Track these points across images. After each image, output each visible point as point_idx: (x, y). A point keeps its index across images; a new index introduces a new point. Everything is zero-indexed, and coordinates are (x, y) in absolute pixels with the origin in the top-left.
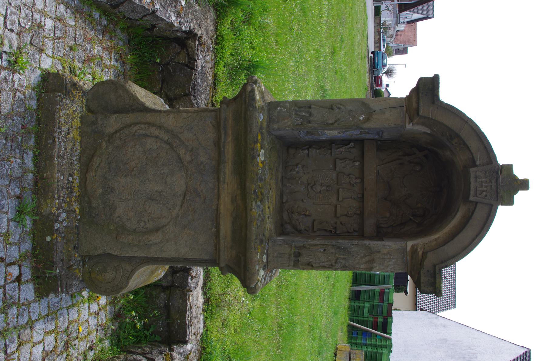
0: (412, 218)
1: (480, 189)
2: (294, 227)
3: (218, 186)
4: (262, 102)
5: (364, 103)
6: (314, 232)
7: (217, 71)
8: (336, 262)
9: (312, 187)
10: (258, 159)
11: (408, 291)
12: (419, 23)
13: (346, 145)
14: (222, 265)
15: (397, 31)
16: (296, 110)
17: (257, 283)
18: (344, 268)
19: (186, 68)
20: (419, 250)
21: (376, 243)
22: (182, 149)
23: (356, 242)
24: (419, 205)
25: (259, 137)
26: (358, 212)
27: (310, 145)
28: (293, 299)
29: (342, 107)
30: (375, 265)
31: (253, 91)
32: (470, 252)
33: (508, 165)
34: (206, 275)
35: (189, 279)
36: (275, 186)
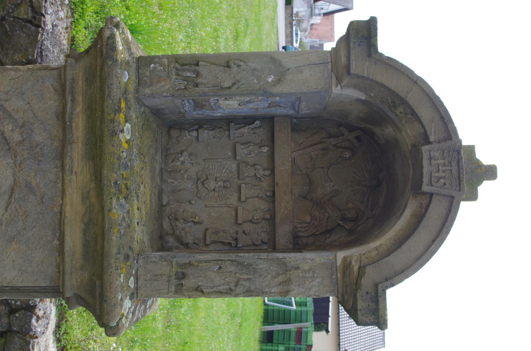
0: (341, 223)
1: (437, 174)
2: (179, 240)
3: (63, 177)
4: (127, 55)
5: (274, 58)
6: (207, 245)
7: (74, 32)
8: (236, 285)
9: (203, 183)
10: (121, 135)
11: (330, 329)
12: (336, 15)
13: (250, 124)
14: (68, 294)
15: (312, 25)
16: (177, 69)
17: (121, 319)
18: (249, 293)
19: (29, 25)
20: (353, 263)
21: (293, 255)
22: (8, 124)
23: (264, 255)
24: (350, 205)
25: (123, 105)
26: (268, 216)
27: (200, 124)
28: (187, 343)
29: (242, 63)
30: (292, 287)
31: (112, 37)
32: (424, 264)
33: (469, 146)
34: (60, 314)
35: (34, 321)
36: (149, 181)
